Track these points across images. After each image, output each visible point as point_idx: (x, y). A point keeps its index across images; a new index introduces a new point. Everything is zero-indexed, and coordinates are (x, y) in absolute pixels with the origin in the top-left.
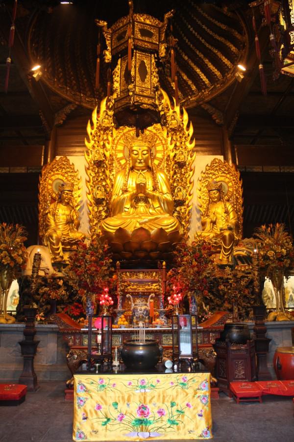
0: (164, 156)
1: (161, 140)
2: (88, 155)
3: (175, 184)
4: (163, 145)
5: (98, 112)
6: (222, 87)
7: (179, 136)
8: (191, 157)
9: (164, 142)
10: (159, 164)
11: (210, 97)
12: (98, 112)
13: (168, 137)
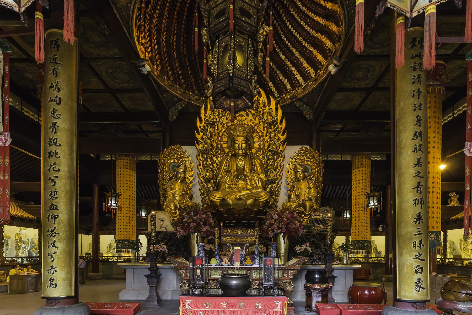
0: (260, 146)
1: (259, 133)
2: (199, 145)
3: (269, 167)
4: (260, 137)
5: (206, 109)
6: (314, 84)
7: (273, 130)
8: (282, 146)
9: (260, 134)
10: (256, 152)
11: (303, 94)
12: (206, 109)
13: (264, 130)
